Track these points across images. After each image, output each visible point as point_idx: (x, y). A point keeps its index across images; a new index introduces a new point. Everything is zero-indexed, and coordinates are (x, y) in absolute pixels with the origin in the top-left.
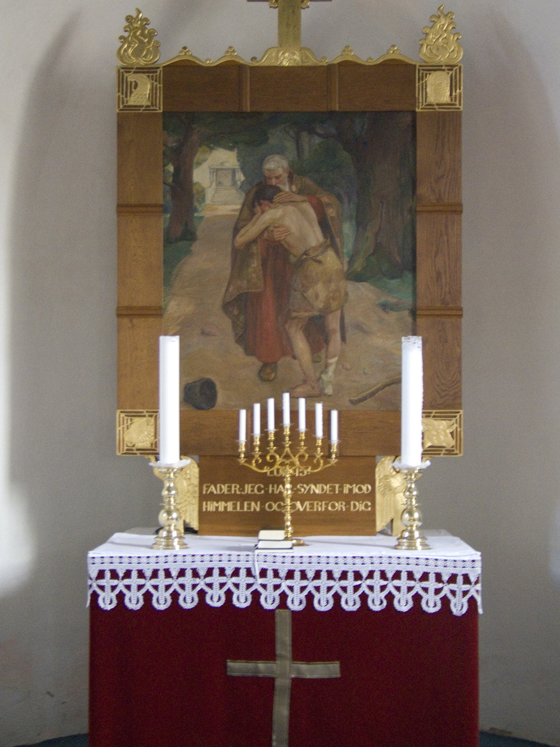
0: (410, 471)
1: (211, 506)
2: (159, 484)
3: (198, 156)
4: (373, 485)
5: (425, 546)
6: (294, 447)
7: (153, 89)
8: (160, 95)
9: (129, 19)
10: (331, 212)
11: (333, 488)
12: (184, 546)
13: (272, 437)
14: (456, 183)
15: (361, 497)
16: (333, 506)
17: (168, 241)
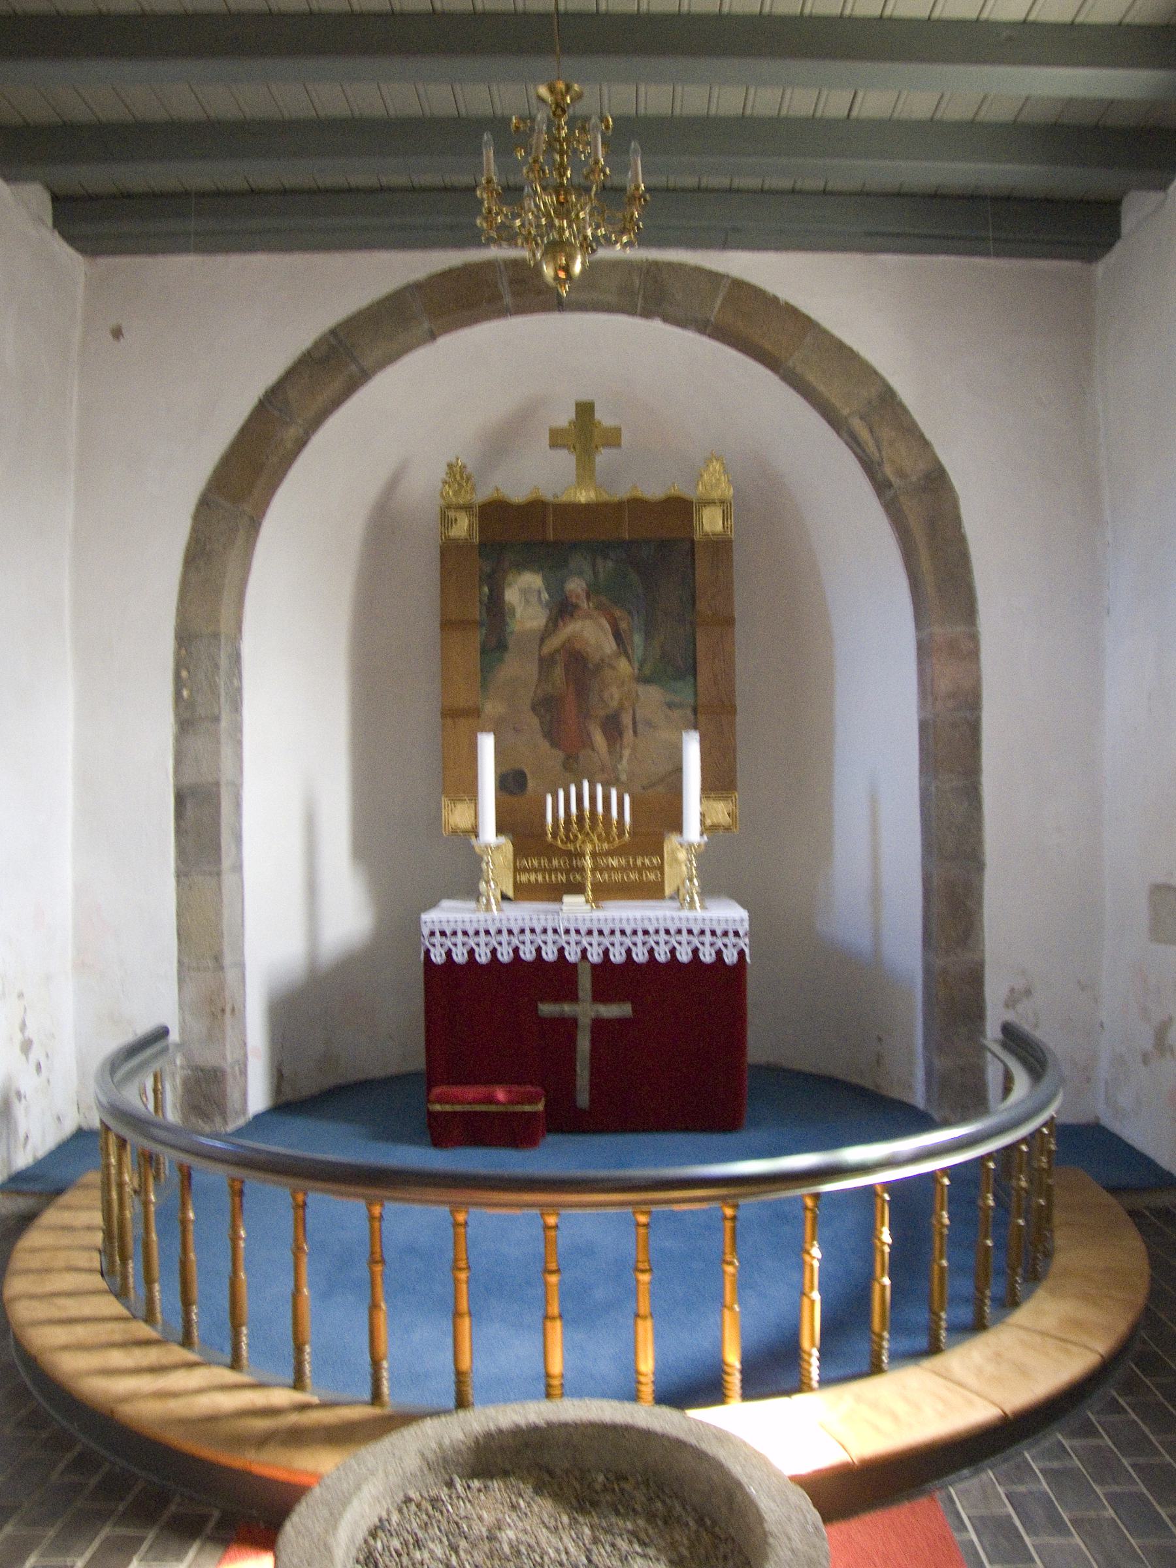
0: (691, 845)
1: (524, 878)
2: (479, 859)
3: (510, 578)
4: (662, 858)
5: (703, 907)
6: (593, 827)
7: (470, 525)
8: (476, 528)
9: (450, 466)
10: (623, 625)
11: (628, 862)
12: (500, 909)
13: (574, 818)
14: (729, 598)
15: (652, 868)
16: (628, 876)
17: (484, 651)
